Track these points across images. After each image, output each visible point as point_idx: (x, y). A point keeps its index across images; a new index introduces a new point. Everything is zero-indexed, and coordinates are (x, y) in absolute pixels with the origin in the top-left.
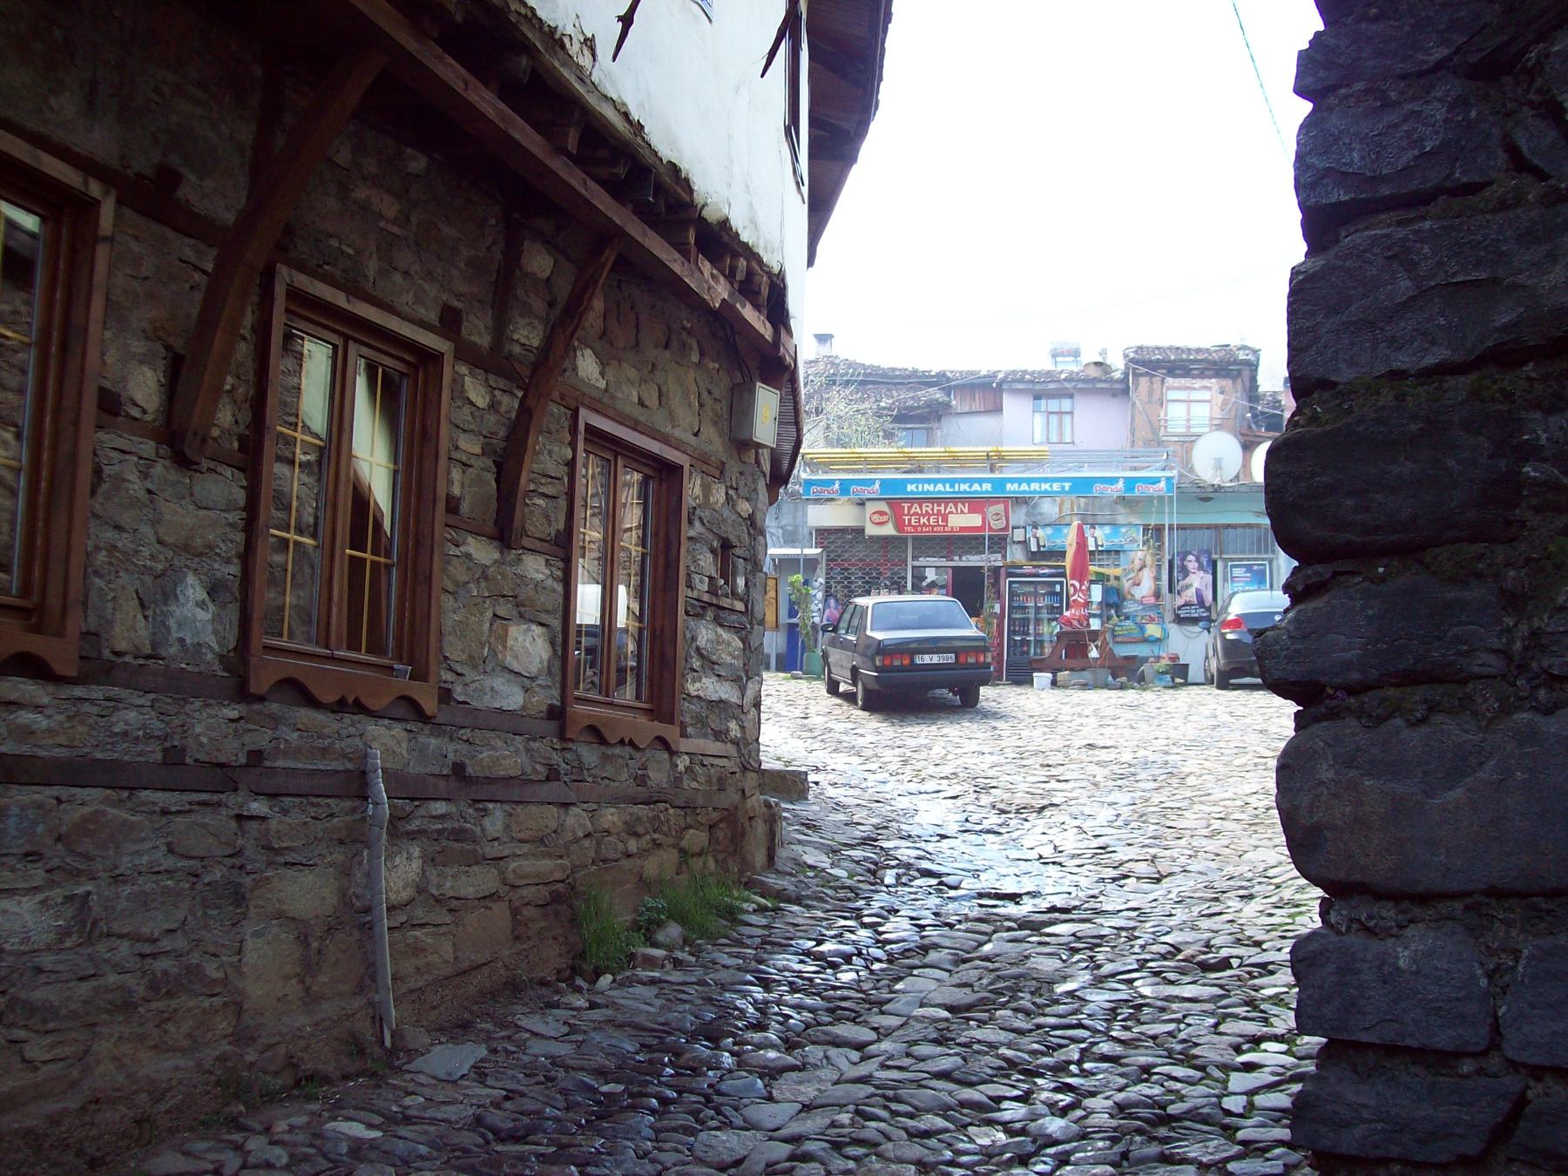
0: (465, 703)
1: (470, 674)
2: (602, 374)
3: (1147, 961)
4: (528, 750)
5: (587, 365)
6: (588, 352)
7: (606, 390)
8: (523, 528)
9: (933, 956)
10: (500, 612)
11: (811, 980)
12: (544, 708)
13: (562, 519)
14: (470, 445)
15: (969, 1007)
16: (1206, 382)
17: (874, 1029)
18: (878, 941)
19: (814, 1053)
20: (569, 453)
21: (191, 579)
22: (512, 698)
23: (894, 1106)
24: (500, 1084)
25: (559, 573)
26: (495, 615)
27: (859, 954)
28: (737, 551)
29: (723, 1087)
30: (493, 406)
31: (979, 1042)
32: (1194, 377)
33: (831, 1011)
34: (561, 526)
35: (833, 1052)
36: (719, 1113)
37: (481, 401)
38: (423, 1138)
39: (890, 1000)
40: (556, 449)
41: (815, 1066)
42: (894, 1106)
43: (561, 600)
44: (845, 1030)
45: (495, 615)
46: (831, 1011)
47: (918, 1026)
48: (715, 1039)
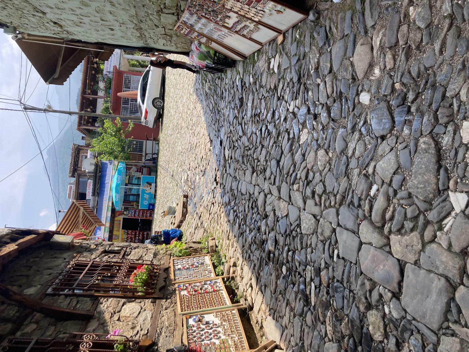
0: (148, 330)
1: (138, 328)
2: (35, 286)
3: (239, 123)
4: (166, 309)
5: (31, 291)
6: (25, 291)
7: (42, 285)
8: (88, 310)
9: (234, 187)
10: (117, 318)
11: (242, 219)
12: (152, 304)
13: (86, 299)
14: (51, 331)
15: (253, 168)
16: (80, 157)
17: (259, 193)
18: (229, 204)
19: (268, 208)
20: (63, 296)
21: (73, 346)
22: (148, 314)
23: (291, 172)
24: (284, 310)
25: (105, 299)
26: (118, 320)
27: (233, 208)
28: (107, 249)
29: (283, 232)
30: (37, 322)
31: (265, 158)
32: (79, 159)
33: (252, 208)
34: (89, 299)
35: (268, 202)
36: (294, 230)
37: (34, 326)
38: (311, 334)
39: (249, 193)
40: (60, 301)
41: (273, 207)
42: (291, 172)
43: (115, 299)
44: (260, 203)
45: (118, 320)
46: (252, 208)
47: (259, 180)
48: (263, 242)
